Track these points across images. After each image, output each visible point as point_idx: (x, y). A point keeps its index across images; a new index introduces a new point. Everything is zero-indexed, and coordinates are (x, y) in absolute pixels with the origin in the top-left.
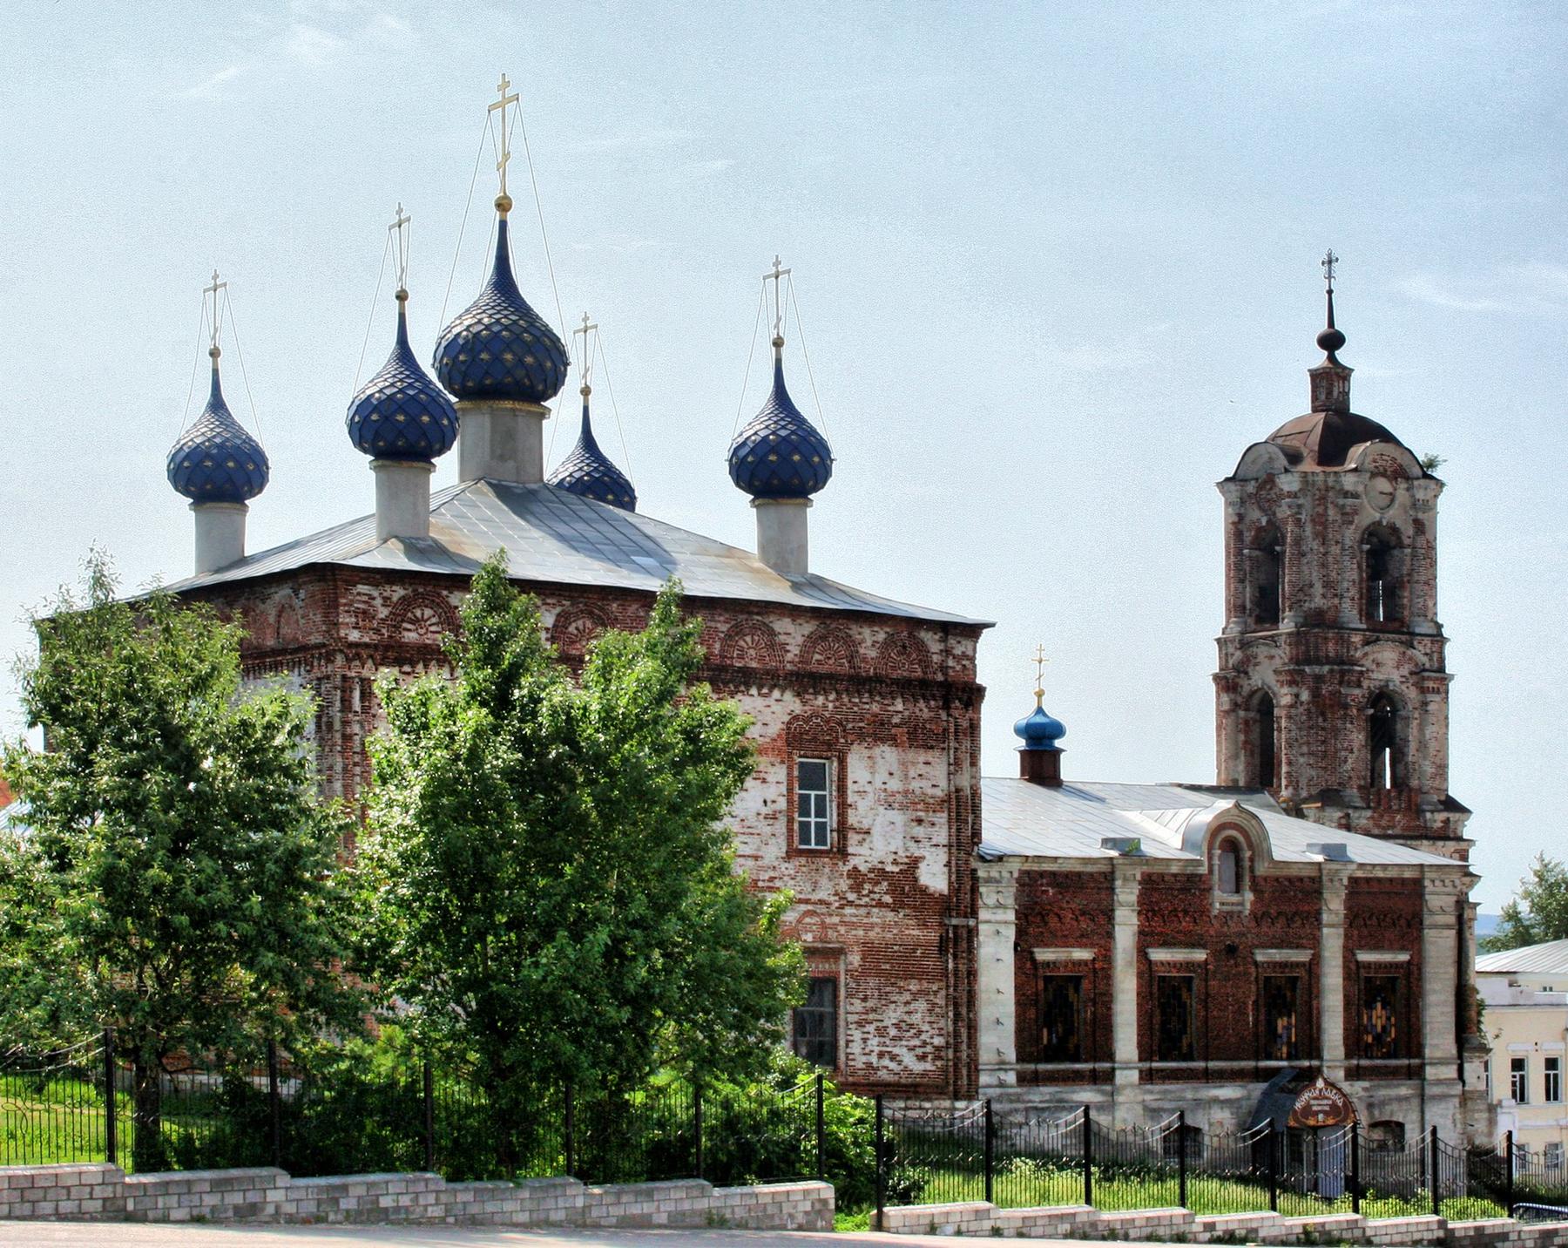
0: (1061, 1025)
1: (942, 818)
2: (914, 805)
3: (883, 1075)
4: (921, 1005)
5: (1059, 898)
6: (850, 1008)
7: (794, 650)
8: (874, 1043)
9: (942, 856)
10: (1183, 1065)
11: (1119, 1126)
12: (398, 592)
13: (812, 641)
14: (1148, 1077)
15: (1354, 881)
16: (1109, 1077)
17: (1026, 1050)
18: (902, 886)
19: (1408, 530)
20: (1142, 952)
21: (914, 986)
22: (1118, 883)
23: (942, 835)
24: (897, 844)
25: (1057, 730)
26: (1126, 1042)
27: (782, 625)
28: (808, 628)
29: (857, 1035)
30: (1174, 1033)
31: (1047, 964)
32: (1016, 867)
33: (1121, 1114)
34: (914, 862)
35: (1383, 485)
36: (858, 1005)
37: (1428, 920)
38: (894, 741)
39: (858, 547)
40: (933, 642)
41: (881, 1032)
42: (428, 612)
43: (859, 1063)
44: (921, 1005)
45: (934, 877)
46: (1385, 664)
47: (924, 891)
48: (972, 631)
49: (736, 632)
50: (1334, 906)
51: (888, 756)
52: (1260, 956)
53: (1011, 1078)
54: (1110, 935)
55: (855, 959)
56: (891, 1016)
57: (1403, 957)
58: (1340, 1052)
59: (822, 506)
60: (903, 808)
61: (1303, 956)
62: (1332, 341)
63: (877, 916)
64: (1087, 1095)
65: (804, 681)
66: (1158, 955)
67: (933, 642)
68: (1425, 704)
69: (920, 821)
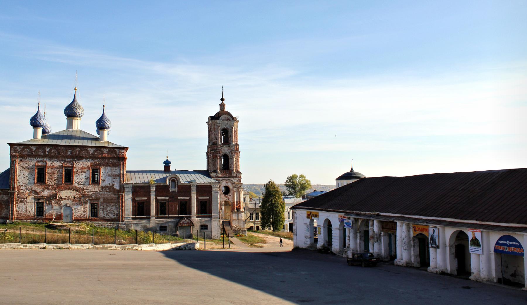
0: (141, 210)
2: (114, 176)
3: (107, 218)
4: (114, 207)
5: (140, 190)
6: (100, 208)
7: (91, 153)
8: (105, 213)
9: (118, 184)
10: (478, 222)
11: (151, 226)
12: (22, 147)
13: (95, 151)
14: (157, 218)
15: (197, 186)
16: (149, 218)
17: (134, 213)
18: (111, 188)
20: (197, 198)
21: (113, 204)
23: (118, 180)
24: (110, 182)
25: (170, 163)
26: (194, 209)
27: (89, 149)
28: (94, 149)
29: (102, 212)
30: (162, 210)
31: (138, 200)
32: (131, 185)
33: (151, 224)
34: (113, 185)
35: (226, 122)
36: (102, 207)
38: (110, 166)
39: (111, 138)
40: (117, 150)
41: (107, 211)
43: (102, 216)
44: (114, 207)
45: (117, 187)
46: (226, 150)
47: (115, 189)
48: (126, 149)
49: (81, 150)
50: (153, 189)
51: (109, 168)
52: (179, 198)
53: (131, 218)
54: (150, 195)
55: (102, 200)
56: (108, 209)
57: (208, 198)
59: (106, 132)
60: (111, 176)
61: (188, 198)
62: (222, 100)
63: (106, 193)
64: (144, 221)
65: (93, 157)
66: (159, 198)
67: (117, 150)
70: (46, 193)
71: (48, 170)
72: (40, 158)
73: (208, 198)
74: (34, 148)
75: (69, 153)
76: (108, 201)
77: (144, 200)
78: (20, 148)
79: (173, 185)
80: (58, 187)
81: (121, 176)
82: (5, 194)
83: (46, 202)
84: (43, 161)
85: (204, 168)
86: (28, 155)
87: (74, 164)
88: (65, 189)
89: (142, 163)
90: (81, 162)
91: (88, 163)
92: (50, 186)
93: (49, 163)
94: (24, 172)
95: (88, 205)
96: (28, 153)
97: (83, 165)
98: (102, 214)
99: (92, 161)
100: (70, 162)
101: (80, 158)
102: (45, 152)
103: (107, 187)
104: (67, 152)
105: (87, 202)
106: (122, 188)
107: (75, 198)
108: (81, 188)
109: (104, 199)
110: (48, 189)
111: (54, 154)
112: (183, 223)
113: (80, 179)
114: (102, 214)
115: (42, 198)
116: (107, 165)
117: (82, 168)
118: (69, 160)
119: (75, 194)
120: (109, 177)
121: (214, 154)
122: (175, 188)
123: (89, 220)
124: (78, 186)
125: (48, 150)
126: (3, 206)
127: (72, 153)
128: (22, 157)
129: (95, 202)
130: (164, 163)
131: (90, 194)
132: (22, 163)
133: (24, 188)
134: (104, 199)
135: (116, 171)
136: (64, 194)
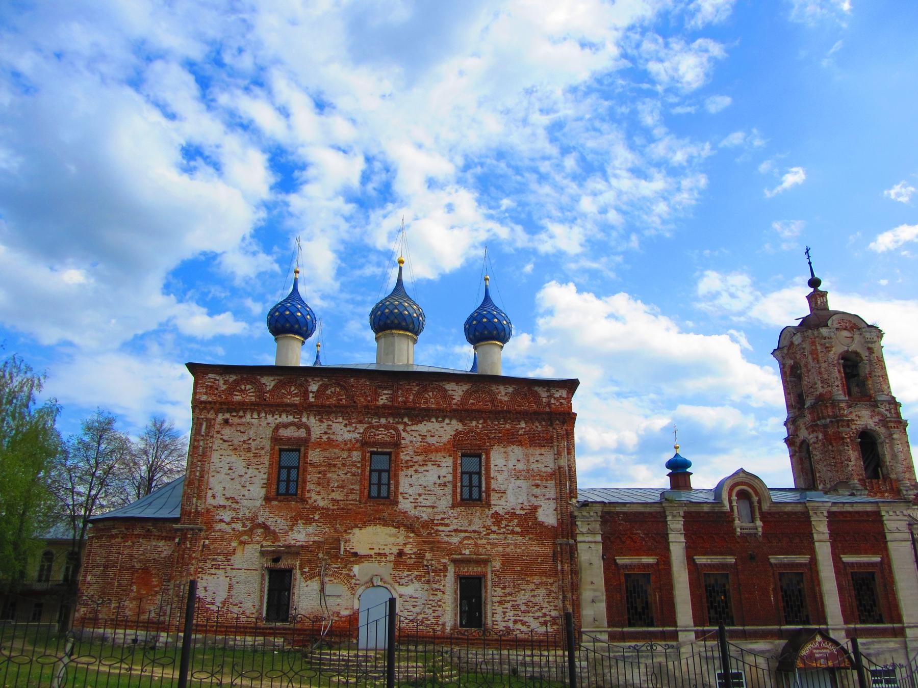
1: (551, 484)
2: (535, 478)
4: (542, 591)
6: (492, 594)
9: (553, 505)
13: (467, 395)
16: (674, 636)
18: (527, 521)
19: (864, 354)
21: (537, 580)
22: (669, 518)
23: (552, 492)
24: (523, 498)
25: (687, 464)
28: (465, 387)
29: (499, 610)
32: (599, 509)
34: (535, 509)
35: (845, 333)
36: (499, 591)
37: (889, 537)
38: (520, 443)
40: (543, 393)
41: (515, 607)
42: (248, 387)
43: (501, 626)
44: (542, 591)
45: (548, 516)
46: (864, 418)
47: (541, 524)
48: (571, 385)
51: (517, 451)
52: (773, 559)
55: (497, 564)
56: (522, 598)
58: (840, 619)
60: (526, 478)
62: (814, 283)
65: (462, 413)
67: (543, 393)
68: (891, 435)
69: (537, 486)
70: (301, 535)
71: (314, 456)
72: (288, 413)
73: (877, 559)
74: (269, 382)
75: (383, 400)
76: (518, 569)
77: (648, 566)
78: (226, 382)
79: (746, 511)
80: (345, 517)
81: (564, 477)
82: (165, 538)
83: (301, 568)
84: (299, 426)
85: (792, 485)
86: (252, 404)
87: (399, 435)
88: (365, 524)
89: (613, 453)
90: (423, 428)
91: (443, 431)
92: (316, 508)
93: (316, 427)
94: (234, 458)
95: (449, 583)
96: (251, 397)
97: (429, 440)
98: (498, 617)
99: (460, 427)
100: (386, 427)
101: (421, 415)
102: (306, 394)
103: (513, 515)
104: (376, 395)
105: (445, 570)
106: (567, 527)
107: (401, 554)
108: (425, 517)
109: (507, 559)
110: (308, 521)
111: (333, 401)
112: (811, 656)
113: (425, 486)
114: (498, 616)
115: (293, 551)
116: (511, 439)
117: (427, 450)
118: (383, 421)
119: (401, 540)
120: (518, 483)
121: (830, 431)
122: (753, 520)
123: (450, 640)
124: (413, 513)
125: (314, 387)
126: (155, 581)
127: (393, 398)
128: (230, 411)
129: (472, 570)
130: (670, 465)
131: (455, 540)
132: (227, 432)
133: (227, 516)
134: (507, 559)
135: (544, 460)
136: (367, 539)
